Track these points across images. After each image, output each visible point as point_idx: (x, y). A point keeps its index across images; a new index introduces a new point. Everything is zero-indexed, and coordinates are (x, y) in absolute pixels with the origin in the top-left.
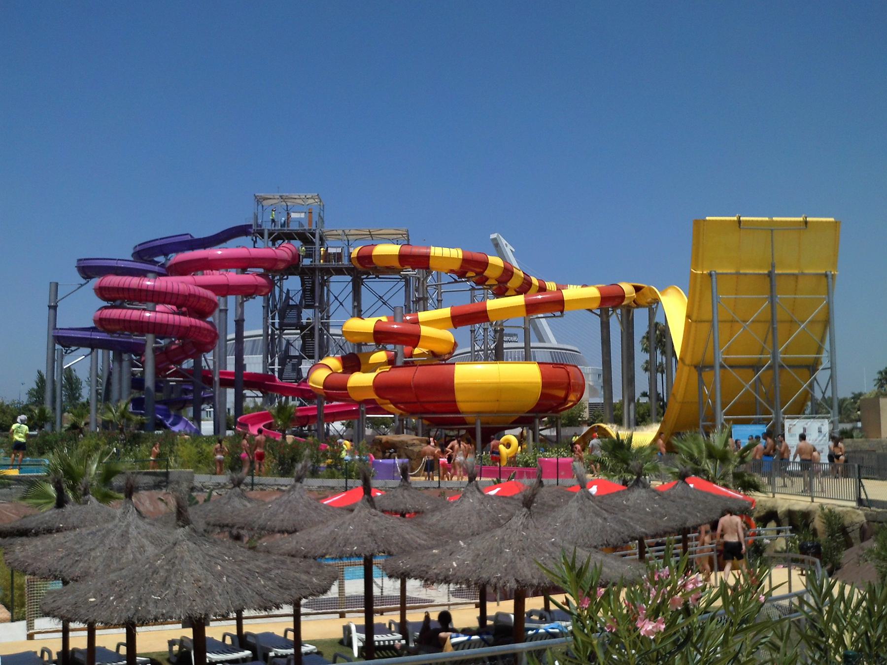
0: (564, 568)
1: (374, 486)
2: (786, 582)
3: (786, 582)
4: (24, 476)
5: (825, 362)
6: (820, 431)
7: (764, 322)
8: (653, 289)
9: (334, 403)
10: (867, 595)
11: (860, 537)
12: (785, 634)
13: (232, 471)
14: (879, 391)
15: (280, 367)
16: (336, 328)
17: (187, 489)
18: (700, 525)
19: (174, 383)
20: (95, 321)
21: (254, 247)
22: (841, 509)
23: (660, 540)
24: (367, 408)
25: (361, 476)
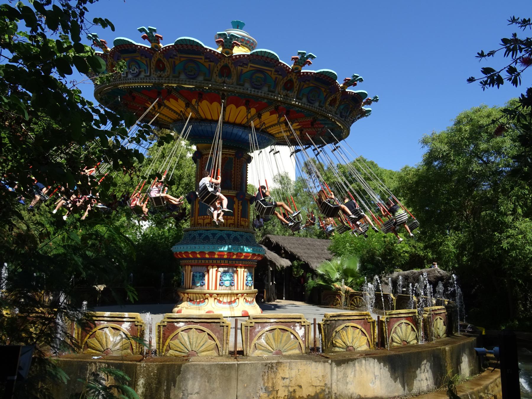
0: (421, 325)
1: (234, 121)
2: (1, 50)
3: (1, 50)
4: (82, 361)
5: (244, 357)
6: (163, 156)
7: (269, 330)
8: (117, 40)
9: (340, 125)
10: (106, 109)
11: (203, 244)
12: (248, 347)
13: (500, 148)
14: (81, 227)
15: (133, 151)
16: (193, 315)
17: (357, 364)
18: (300, 357)
19: (190, 127)
20: (277, 243)
21: (332, 152)
22: (92, 344)
23: (358, 196)
24: (468, 395)
25: (161, 81)
